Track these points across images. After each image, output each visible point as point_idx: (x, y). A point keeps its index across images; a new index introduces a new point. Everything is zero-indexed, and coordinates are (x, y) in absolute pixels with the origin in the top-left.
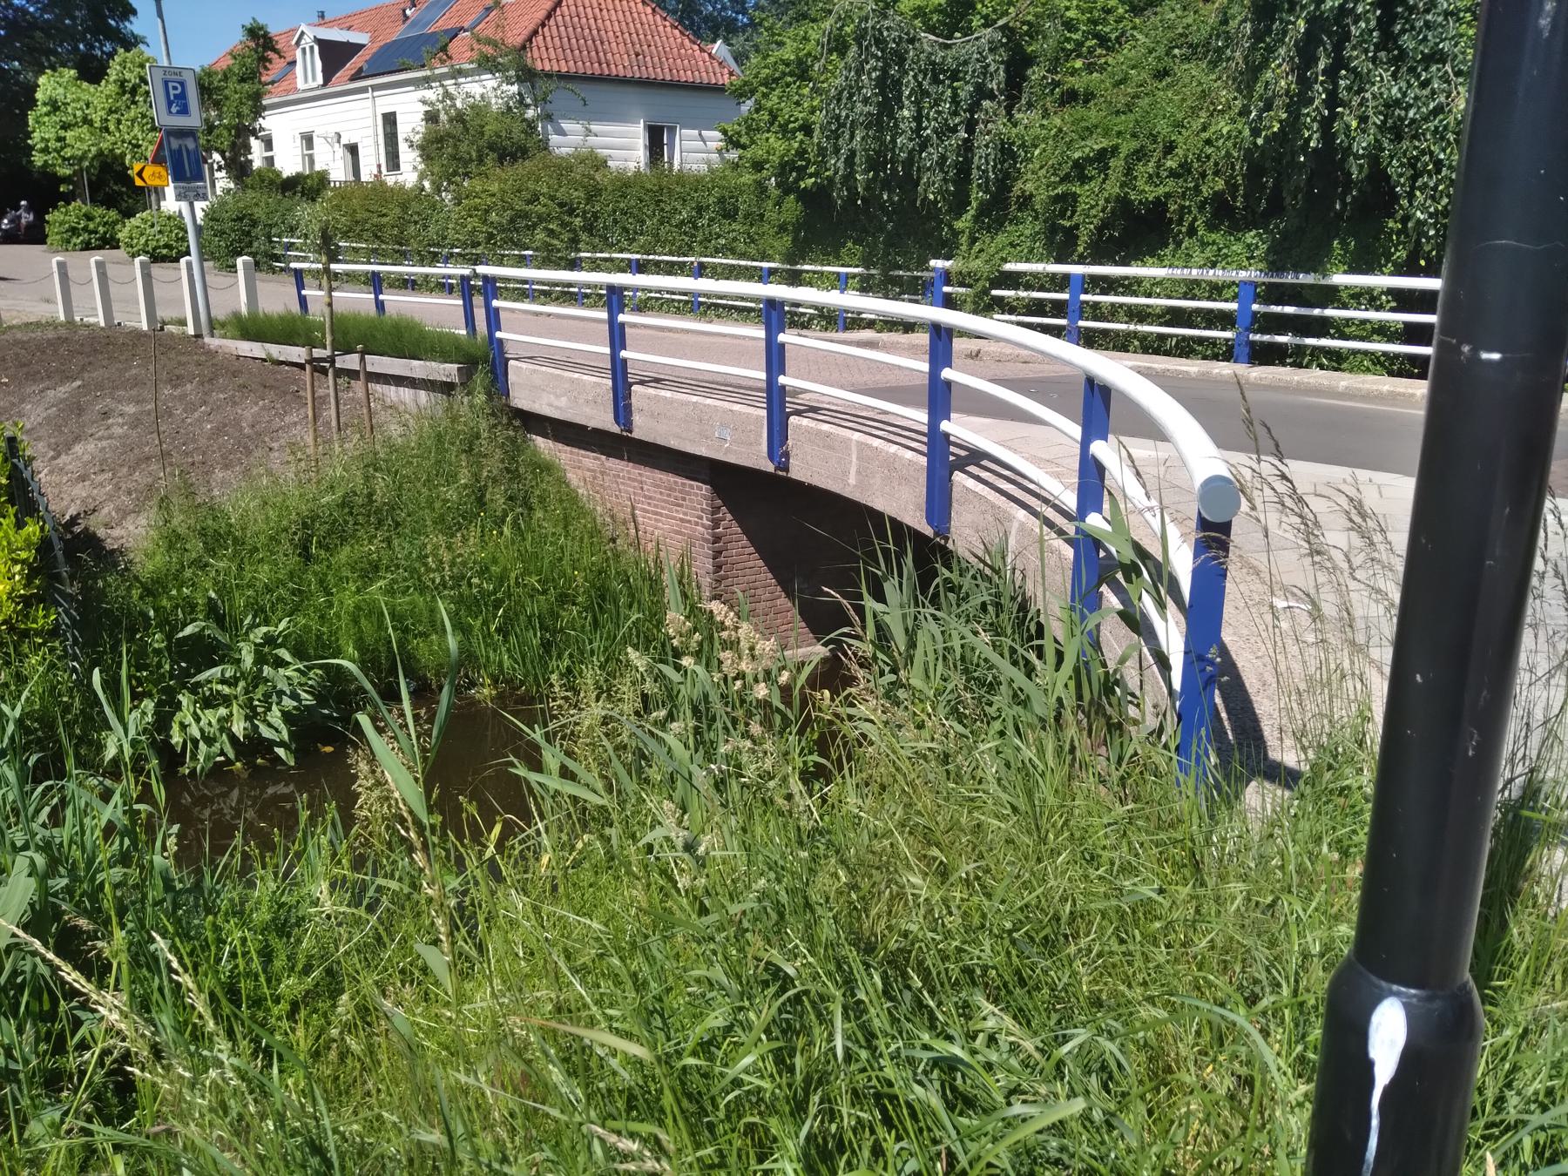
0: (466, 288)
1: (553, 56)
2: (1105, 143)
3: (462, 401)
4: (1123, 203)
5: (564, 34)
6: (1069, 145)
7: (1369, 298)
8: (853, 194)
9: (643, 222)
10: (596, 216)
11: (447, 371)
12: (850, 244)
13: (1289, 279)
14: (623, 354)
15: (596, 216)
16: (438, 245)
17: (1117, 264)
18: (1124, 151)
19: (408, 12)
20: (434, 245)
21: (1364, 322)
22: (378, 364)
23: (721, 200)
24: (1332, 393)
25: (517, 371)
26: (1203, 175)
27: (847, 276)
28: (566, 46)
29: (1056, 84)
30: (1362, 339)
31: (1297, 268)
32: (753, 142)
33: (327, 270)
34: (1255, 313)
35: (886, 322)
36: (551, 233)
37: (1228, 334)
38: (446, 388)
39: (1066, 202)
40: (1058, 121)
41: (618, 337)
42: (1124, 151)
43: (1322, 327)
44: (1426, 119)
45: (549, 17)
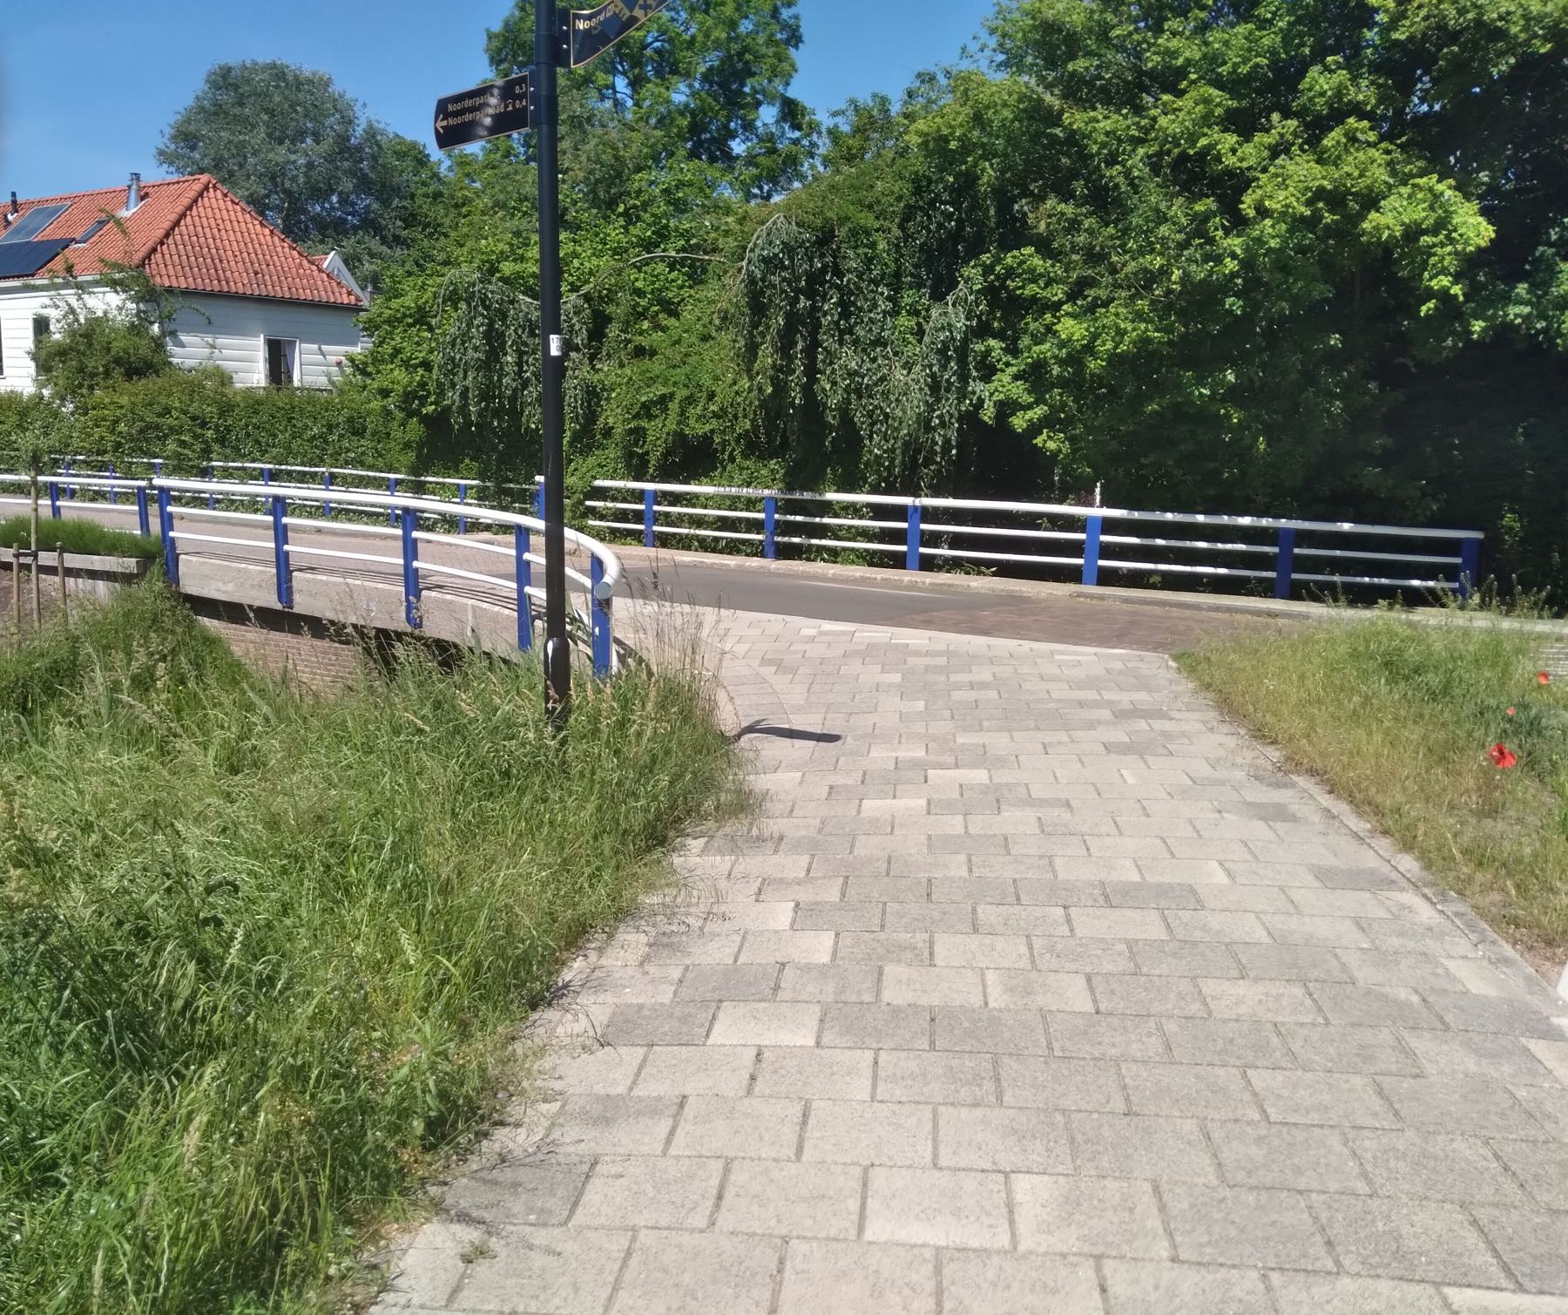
0: (142, 498)
1: (172, 272)
2: (664, 390)
3: (141, 590)
4: (680, 437)
5: (182, 252)
6: (638, 390)
7: (853, 510)
8: (468, 424)
9: (275, 436)
10: (228, 429)
11: (130, 564)
12: (467, 461)
13: (797, 496)
14: (286, 547)
15: (228, 429)
16: (60, 452)
17: (681, 482)
18: (678, 397)
19: (10, 217)
20: (55, 452)
21: (850, 527)
22: (73, 560)
23: (350, 420)
24: (825, 579)
25: (187, 565)
26: (736, 417)
27: (467, 487)
28: (185, 263)
29: (629, 341)
30: (849, 540)
31: (803, 489)
32: (378, 372)
33: (35, 483)
34: (777, 522)
35: (501, 526)
36: (183, 444)
37: (760, 537)
38: (127, 578)
39: (638, 434)
40: (628, 372)
41: (281, 534)
42: (678, 397)
43: (823, 531)
44: (876, 384)
45: (167, 235)
